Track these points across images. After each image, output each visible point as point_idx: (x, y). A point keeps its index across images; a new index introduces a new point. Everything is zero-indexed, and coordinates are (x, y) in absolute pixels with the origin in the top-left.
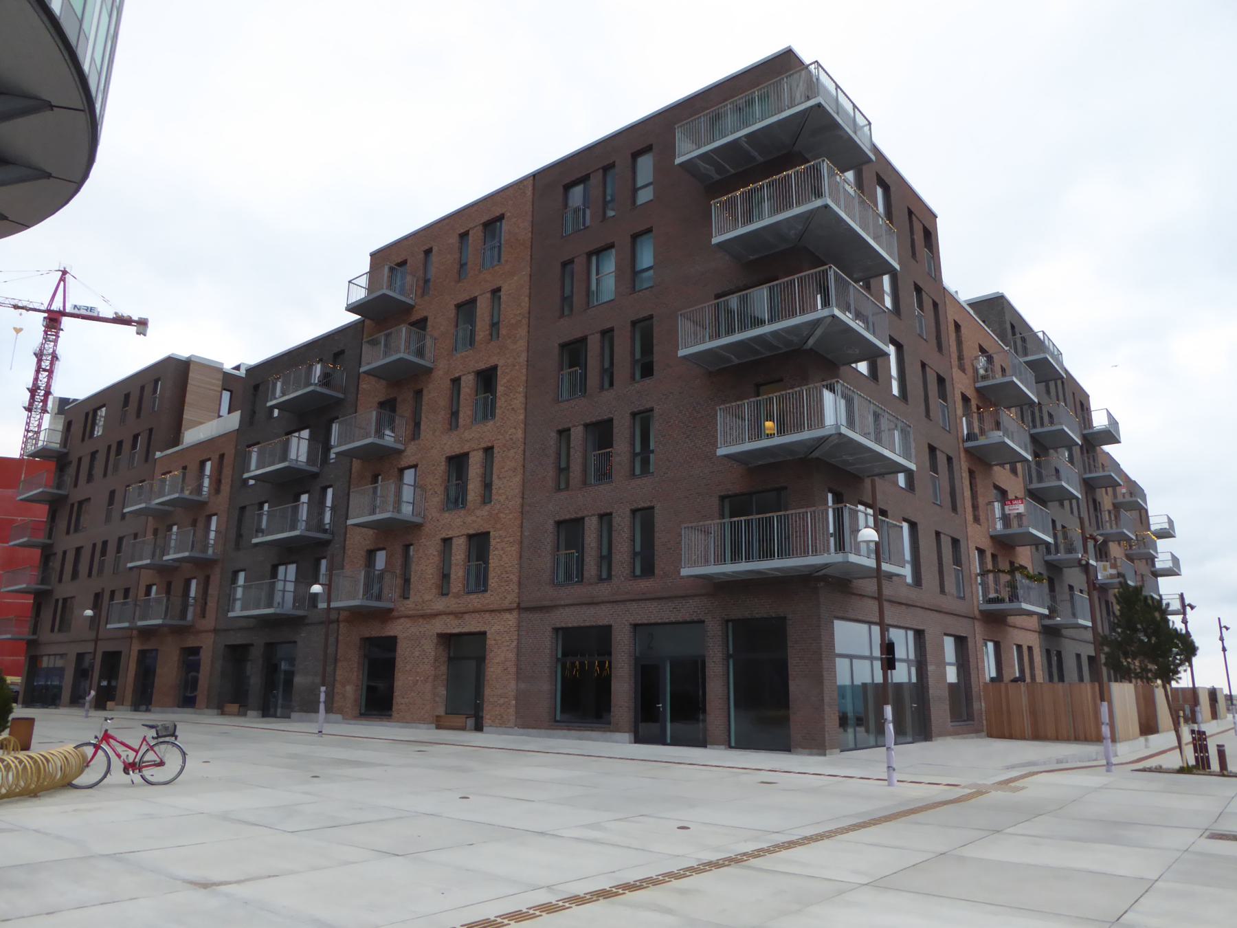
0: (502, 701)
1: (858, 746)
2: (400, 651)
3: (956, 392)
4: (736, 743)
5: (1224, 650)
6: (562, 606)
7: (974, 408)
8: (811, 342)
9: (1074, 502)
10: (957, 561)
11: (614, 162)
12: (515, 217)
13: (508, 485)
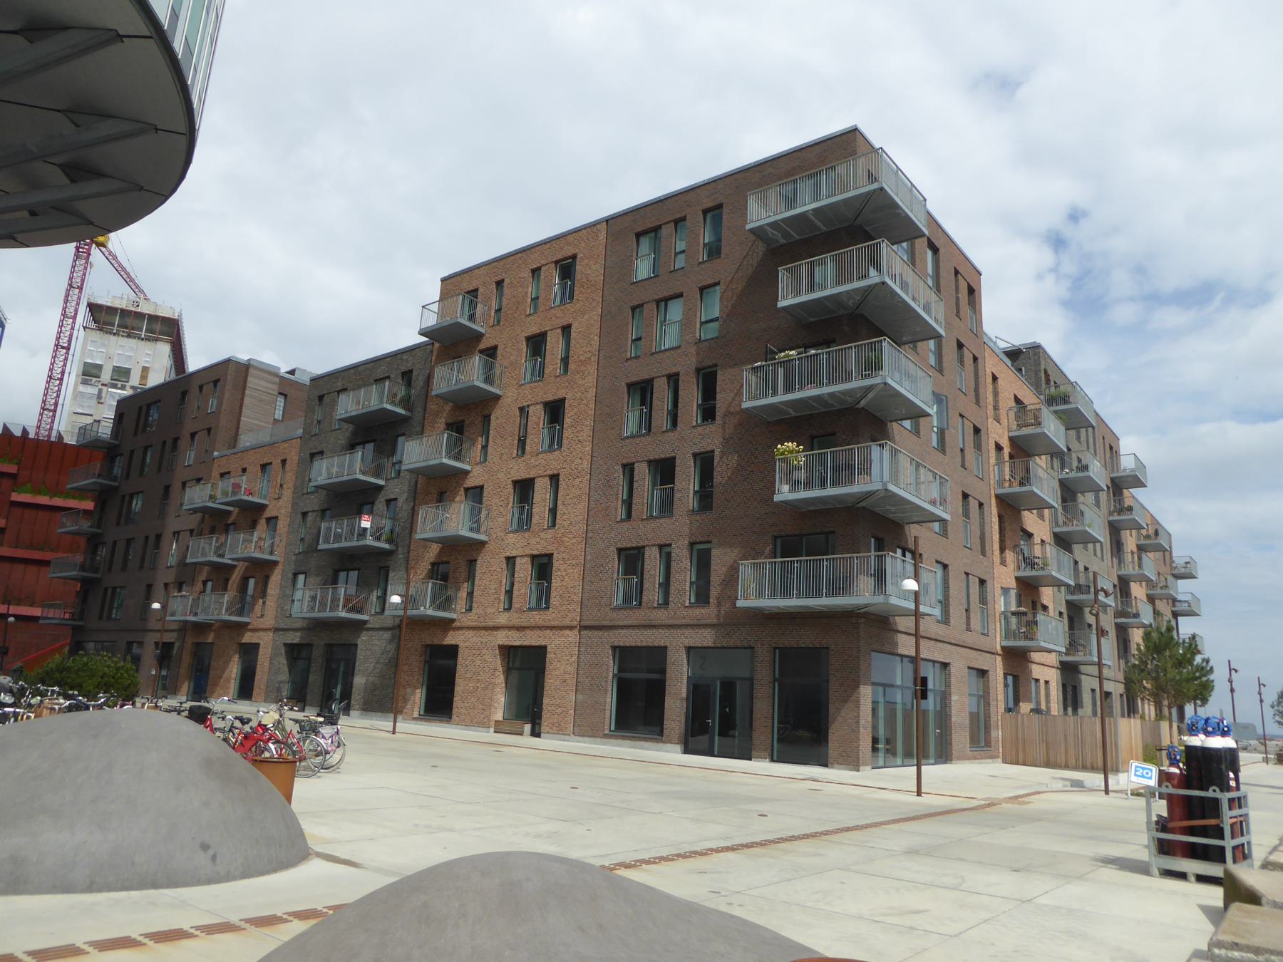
0: (559, 710)
1: (887, 765)
2: (460, 659)
3: (990, 442)
4: (777, 758)
5: (1232, 690)
6: (620, 626)
7: (1007, 458)
8: (863, 403)
9: (1098, 545)
10: (983, 600)
11: (686, 216)
12: (588, 259)
13: (573, 511)
